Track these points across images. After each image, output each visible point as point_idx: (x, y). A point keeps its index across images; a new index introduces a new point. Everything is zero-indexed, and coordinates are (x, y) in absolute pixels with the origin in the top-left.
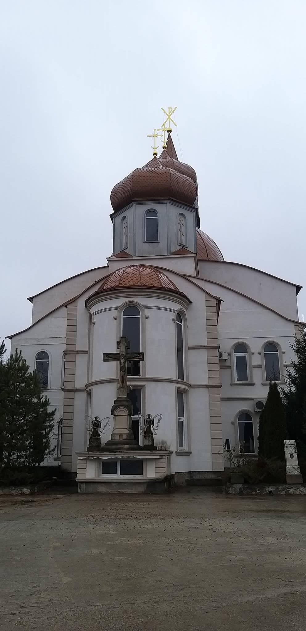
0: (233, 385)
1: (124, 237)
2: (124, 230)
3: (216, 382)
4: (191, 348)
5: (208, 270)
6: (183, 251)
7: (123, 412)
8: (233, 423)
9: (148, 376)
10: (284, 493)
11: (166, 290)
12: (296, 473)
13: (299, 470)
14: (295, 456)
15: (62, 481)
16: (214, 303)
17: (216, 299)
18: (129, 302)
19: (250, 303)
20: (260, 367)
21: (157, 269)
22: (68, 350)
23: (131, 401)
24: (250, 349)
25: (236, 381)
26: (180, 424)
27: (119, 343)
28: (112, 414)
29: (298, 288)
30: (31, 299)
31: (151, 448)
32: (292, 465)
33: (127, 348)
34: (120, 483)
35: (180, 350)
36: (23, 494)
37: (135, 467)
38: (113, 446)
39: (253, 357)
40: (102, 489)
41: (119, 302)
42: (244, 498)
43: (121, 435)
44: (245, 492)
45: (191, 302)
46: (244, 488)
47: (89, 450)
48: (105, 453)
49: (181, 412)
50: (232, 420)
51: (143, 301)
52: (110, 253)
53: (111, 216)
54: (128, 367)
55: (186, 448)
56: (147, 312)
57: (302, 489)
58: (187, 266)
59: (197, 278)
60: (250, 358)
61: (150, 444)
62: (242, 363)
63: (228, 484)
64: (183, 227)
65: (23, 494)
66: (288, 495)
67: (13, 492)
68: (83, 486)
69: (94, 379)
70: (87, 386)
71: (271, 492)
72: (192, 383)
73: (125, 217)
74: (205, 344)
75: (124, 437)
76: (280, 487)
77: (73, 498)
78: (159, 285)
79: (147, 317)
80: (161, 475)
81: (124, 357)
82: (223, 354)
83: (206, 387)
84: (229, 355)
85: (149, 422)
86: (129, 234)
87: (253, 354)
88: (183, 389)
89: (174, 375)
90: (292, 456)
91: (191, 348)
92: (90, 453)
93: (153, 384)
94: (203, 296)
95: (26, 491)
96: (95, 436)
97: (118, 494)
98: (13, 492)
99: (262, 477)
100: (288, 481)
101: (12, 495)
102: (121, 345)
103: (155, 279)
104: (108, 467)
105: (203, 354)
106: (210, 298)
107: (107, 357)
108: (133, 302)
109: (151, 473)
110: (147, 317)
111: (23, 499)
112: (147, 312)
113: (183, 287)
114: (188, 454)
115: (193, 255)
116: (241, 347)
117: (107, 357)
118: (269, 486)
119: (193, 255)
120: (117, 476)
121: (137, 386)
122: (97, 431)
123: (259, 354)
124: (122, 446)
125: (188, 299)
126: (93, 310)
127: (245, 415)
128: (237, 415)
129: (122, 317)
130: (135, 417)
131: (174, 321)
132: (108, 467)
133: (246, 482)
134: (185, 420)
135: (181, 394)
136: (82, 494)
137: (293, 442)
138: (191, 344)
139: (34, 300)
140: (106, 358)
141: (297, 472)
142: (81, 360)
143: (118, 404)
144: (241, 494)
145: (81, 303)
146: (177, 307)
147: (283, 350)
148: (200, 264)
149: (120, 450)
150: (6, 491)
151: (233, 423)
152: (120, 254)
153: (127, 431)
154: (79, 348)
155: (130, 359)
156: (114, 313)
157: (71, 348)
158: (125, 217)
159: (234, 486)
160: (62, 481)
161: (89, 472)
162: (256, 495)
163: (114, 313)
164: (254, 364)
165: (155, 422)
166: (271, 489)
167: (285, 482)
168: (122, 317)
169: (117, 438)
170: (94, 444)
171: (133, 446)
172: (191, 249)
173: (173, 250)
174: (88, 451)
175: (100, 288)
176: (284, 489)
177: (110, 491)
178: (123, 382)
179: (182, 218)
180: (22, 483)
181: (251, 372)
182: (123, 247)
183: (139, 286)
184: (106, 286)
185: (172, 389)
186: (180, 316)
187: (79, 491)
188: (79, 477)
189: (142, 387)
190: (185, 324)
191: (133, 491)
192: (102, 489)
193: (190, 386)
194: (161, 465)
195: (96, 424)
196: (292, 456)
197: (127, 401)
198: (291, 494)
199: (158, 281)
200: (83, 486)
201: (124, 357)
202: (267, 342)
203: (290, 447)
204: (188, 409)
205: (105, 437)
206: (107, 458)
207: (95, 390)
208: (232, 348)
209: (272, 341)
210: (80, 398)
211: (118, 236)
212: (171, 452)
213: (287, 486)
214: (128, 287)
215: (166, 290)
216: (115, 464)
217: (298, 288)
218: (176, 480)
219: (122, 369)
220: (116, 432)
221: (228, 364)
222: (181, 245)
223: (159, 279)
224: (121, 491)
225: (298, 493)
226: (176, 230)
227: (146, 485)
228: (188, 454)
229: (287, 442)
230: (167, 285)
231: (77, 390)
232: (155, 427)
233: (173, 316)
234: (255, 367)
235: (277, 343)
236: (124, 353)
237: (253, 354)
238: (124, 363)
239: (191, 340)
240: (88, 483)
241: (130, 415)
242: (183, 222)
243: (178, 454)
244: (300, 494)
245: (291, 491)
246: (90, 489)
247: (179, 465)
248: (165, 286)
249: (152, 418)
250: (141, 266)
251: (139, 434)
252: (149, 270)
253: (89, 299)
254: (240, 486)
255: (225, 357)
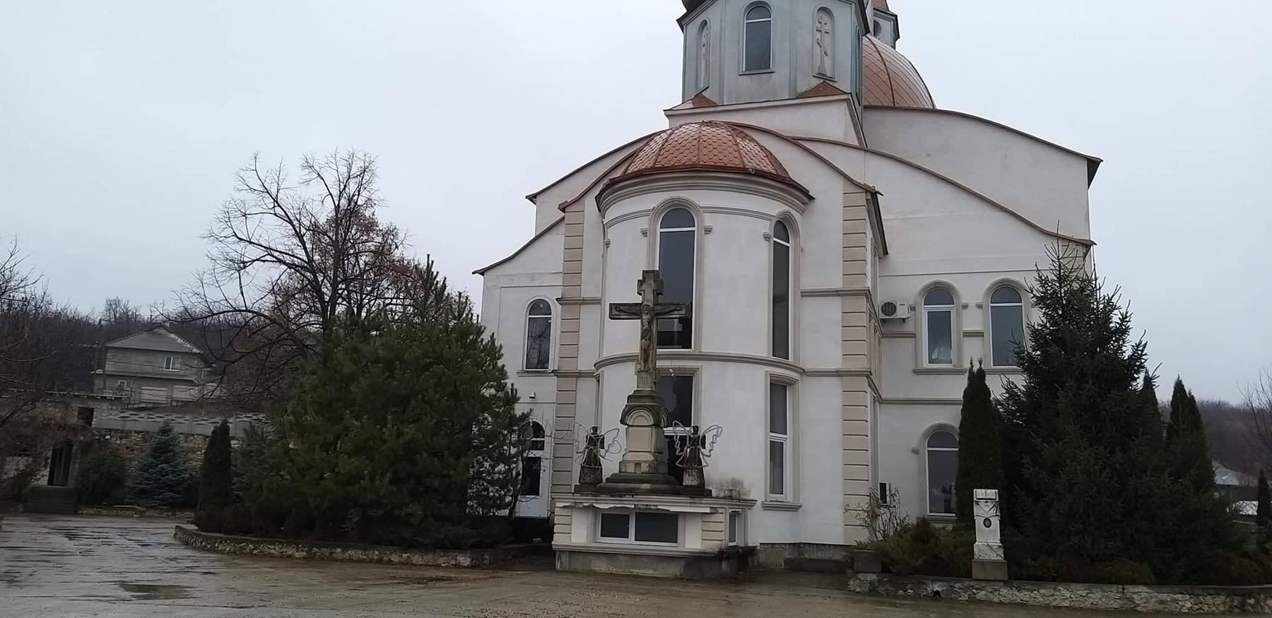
0: (919, 372)
1: (703, 62)
2: (704, 50)
3: (860, 364)
4: (805, 294)
5: (894, 131)
6: (825, 89)
7: (646, 418)
8: (915, 451)
9: (706, 349)
10: (965, 597)
11: (749, 174)
12: (994, 557)
13: (1001, 552)
14: (996, 522)
15: (530, 545)
16: (862, 199)
17: (867, 191)
18: (673, 200)
19: (963, 197)
20: (979, 334)
21: (739, 129)
22: (567, 296)
23: (670, 399)
24: (958, 297)
25: (926, 364)
26: (776, 451)
27: (641, 283)
28: (623, 422)
29: (1093, 165)
30: (532, 198)
31: (700, 491)
32: (988, 540)
33: (657, 293)
34: (634, 556)
35: (780, 301)
36: (457, 566)
37: (665, 526)
38: (622, 484)
39: (965, 313)
40: (600, 566)
41: (653, 200)
42: (881, 603)
43: (638, 464)
44: (881, 589)
45: (811, 198)
46: (880, 581)
47: (578, 490)
48: (603, 497)
49: (777, 420)
50: (914, 443)
51: (700, 198)
52: (675, 100)
53: (680, 21)
54: (659, 333)
55: (788, 496)
56: (708, 220)
57: (1004, 591)
58: (831, 121)
59: (863, 148)
60: (959, 316)
61: (695, 483)
62: (940, 329)
63: (849, 571)
64: (827, 38)
65: (457, 566)
66: (973, 601)
67: (440, 561)
68: (565, 558)
69: (607, 354)
70: (599, 365)
71: (937, 593)
72: (808, 366)
73: (705, 23)
74: (838, 284)
75: (645, 468)
76: (957, 585)
77: (838, 594)
78: (736, 163)
79: (708, 231)
80: (712, 546)
81: (650, 311)
82: (898, 307)
83: (838, 374)
84: (913, 308)
85: (698, 441)
86: (712, 58)
87: (965, 307)
88: (789, 378)
89: (762, 348)
90: (987, 523)
91: (805, 294)
92: (577, 496)
93: (716, 365)
94: (838, 185)
95: (464, 560)
96: (592, 463)
97: (624, 575)
98: (440, 561)
99: (920, 562)
100: (976, 573)
101: (390, 562)
102: (644, 287)
103: (731, 150)
104: (613, 524)
105: (832, 310)
106: (852, 189)
107: (620, 311)
108: (678, 199)
109: (693, 540)
110: (708, 231)
111: (410, 572)
112: (708, 220)
113: (798, 167)
114: (795, 508)
115: (845, 97)
116: (939, 293)
117: (620, 311)
118: (934, 581)
119: (845, 97)
120: (629, 542)
121: (685, 369)
122: (596, 456)
123: (980, 307)
124: (637, 485)
125: (805, 193)
126: (612, 213)
127: (938, 435)
128: (925, 435)
129: (659, 230)
130: (669, 431)
131: (767, 238)
132: (613, 524)
133: (885, 570)
134: (788, 440)
135: (779, 390)
136: (562, 572)
137: (992, 493)
138: (809, 283)
139: (538, 199)
140: (615, 312)
141: (997, 556)
142: (589, 317)
143: (635, 402)
144: (873, 592)
145: (590, 201)
146: (775, 208)
147: (964, 301)
148: (872, 118)
149: (632, 492)
150: (428, 558)
151: (915, 451)
152: (698, 100)
153: (650, 457)
154: (586, 294)
155: (667, 313)
156: (644, 223)
157: (572, 293)
158: (705, 23)
159: (860, 576)
160: (530, 545)
161: (575, 532)
162: (905, 597)
163: (644, 223)
164: (966, 329)
165: (708, 441)
166: (937, 588)
167: (968, 575)
168: (659, 230)
169: (631, 469)
170: (587, 479)
171: (657, 486)
172: (845, 84)
173: (803, 87)
174: (576, 492)
175: (622, 175)
176: (965, 589)
177: (614, 571)
178: (646, 361)
179: (826, 18)
180: (454, 546)
181: (959, 346)
182: (702, 86)
183: (693, 166)
184: (632, 169)
185: (758, 379)
186: (783, 227)
187: (558, 567)
188: (558, 540)
189: (696, 370)
190: (797, 245)
191: (657, 574)
192: (600, 566)
193: (803, 372)
194: (713, 527)
195: (595, 441)
196: (987, 523)
197: (652, 398)
198: (981, 601)
199: (736, 154)
200: (565, 558)
201: (650, 311)
202: (997, 283)
203: (986, 503)
204: (795, 420)
205: (610, 465)
206: (607, 507)
207: (607, 372)
208: (920, 294)
209: (1008, 280)
210: (586, 388)
211: (695, 63)
212: (751, 503)
213: (973, 583)
214: (665, 169)
215: (749, 174)
216: (627, 518)
217: (1093, 165)
218: (762, 558)
219: (645, 334)
220: (629, 457)
221: (909, 328)
222: (821, 75)
223: (739, 151)
224: (636, 571)
225: (996, 600)
226: (810, 46)
227: (683, 563)
228: (795, 508)
229: (979, 493)
230: (756, 161)
231: (580, 375)
232: (705, 451)
233: (766, 227)
234: (968, 334)
235: (1016, 283)
236: (651, 305)
237: (965, 307)
238: (650, 323)
239: (805, 275)
240: (575, 553)
241: (657, 425)
242: (828, 28)
243: (766, 507)
244: (1001, 603)
245: (981, 595)
246: (578, 564)
247: (764, 530)
248: (749, 165)
249: (701, 433)
250: (709, 124)
251: (679, 466)
252: (723, 133)
253: (602, 192)
254: (873, 577)
255: (901, 312)
